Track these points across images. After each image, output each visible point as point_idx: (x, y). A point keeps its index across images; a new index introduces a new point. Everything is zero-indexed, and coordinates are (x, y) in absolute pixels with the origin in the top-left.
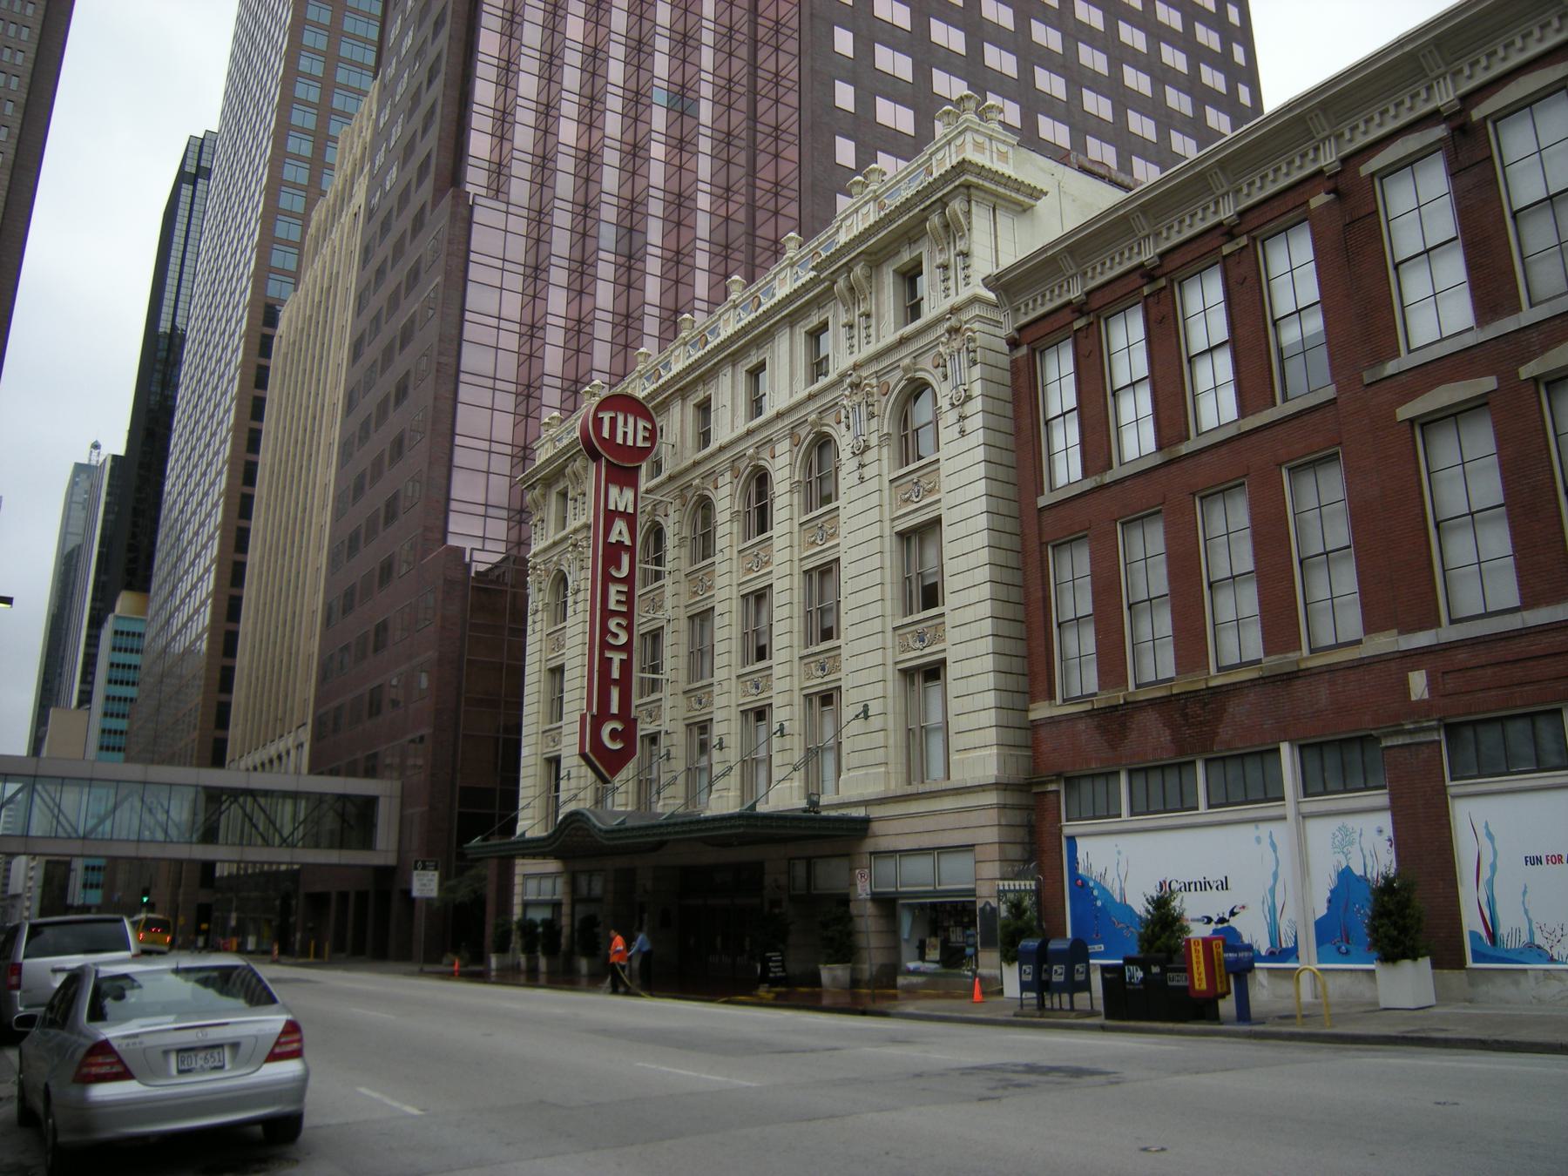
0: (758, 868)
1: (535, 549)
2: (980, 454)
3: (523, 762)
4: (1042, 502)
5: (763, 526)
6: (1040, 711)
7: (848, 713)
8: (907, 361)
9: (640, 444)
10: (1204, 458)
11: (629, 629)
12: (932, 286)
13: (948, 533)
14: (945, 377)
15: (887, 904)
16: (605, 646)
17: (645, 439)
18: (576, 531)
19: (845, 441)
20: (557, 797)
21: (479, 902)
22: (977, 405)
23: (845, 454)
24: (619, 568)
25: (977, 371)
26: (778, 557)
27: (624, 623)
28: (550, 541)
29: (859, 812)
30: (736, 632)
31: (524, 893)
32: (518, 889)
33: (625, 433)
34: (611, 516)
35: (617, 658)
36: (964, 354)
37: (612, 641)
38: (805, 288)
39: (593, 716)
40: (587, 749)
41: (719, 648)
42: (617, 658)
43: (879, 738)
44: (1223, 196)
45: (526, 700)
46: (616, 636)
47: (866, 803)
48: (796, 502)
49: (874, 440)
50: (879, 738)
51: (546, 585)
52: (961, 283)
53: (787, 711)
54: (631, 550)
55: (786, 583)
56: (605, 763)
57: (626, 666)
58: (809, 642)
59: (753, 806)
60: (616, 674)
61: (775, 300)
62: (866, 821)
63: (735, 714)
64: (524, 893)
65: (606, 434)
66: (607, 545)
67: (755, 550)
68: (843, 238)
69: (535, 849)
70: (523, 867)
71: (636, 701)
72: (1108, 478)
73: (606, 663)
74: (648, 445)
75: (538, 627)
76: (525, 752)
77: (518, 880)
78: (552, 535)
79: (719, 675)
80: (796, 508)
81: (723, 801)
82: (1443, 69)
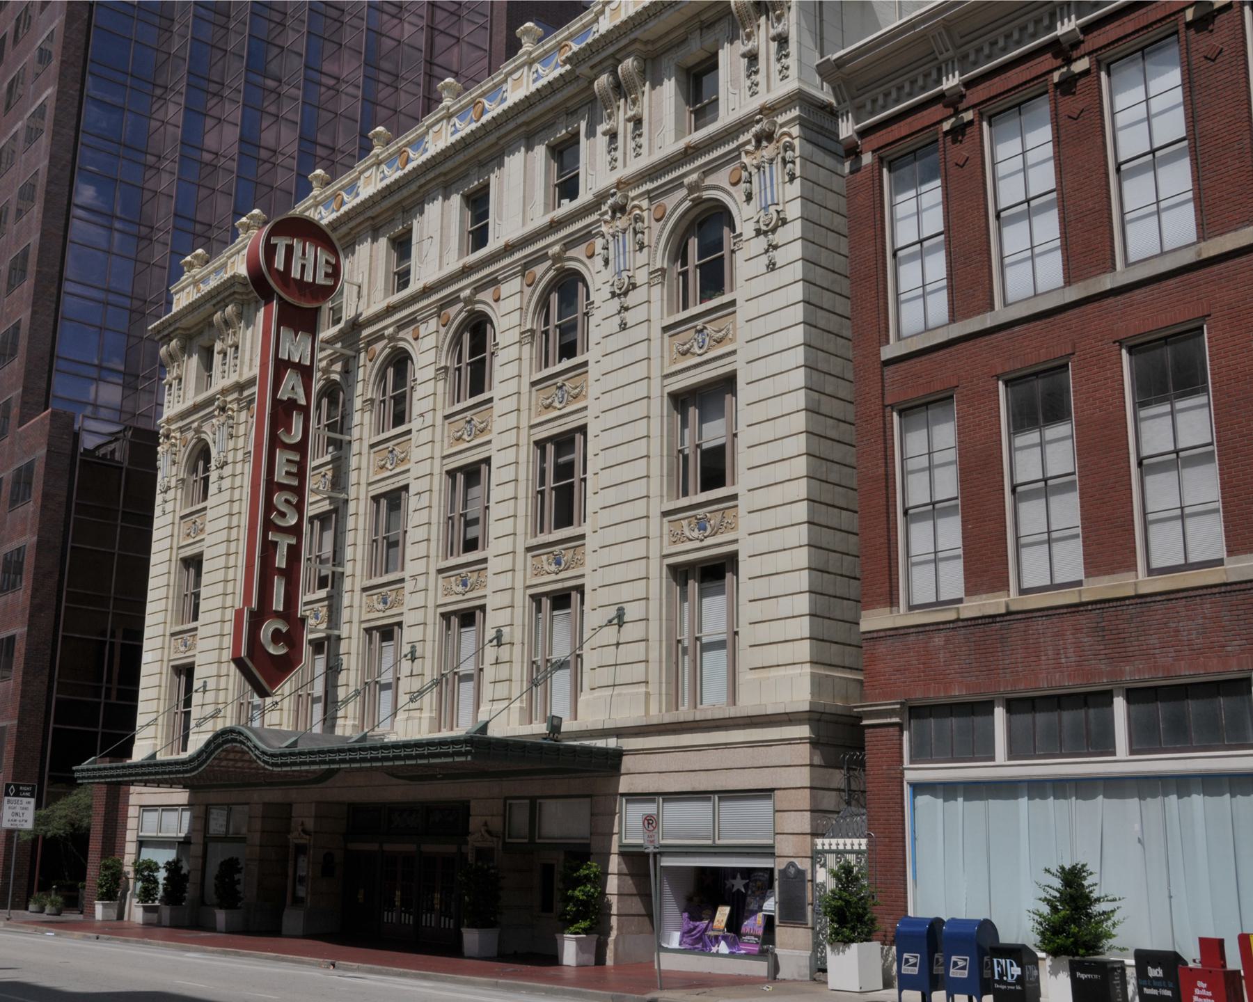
0: (461, 810)
1: (168, 412)
2: (797, 292)
3: (144, 670)
4: (887, 353)
5: (478, 385)
6: (874, 620)
7: (593, 618)
8: (694, 177)
9: (321, 280)
10: (1138, 294)
11: (299, 507)
12: (734, 81)
13: (744, 392)
14: (749, 197)
15: (639, 863)
16: (269, 525)
17: (327, 275)
18: (224, 392)
19: (599, 279)
20: (188, 714)
21: (78, 839)
22: (794, 230)
23: (745, 228)
24: (288, 430)
25: (795, 189)
26: (498, 424)
27: (294, 500)
28: (189, 403)
29: (612, 743)
30: (437, 515)
31: (140, 828)
32: (132, 823)
33: (303, 266)
34: (282, 366)
35: (284, 542)
36: (629, 235)
37: (281, 523)
38: (552, 88)
39: (252, 613)
40: (243, 653)
41: (413, 535)
42: (284, 542)
43: (638, 651)
44: (946, 61)
45: (151, 596)
46: (283, 515)
47: (619, 733)
48: (179, 497)
49: (641, 277)
50: (638, 651)
51: (182, 456)
52: (775, 76)
53: (506, 610)
54: (305, 410)
55: (510, 455)
56: (262, 669)
57: (294, 553)
58: (450, 551)
59: (484, 728)
60: (281, 561)
61: (505, 106)
62: (618, 754)
63: (433, 617)
64: (140, 828)
65: (279, 263)
66: (276, 402)
67: (468, 414)
68: (604, 25)
69: (155, 773)
70: (139, 795)
71: (304, 597)
72: (1107, 282)
73: (269, 548)
74: (330, 282)
75: (169, 507)
76: (146, 657)
77: (132, 812)
78: (192, 397)
79: (411, 568)
80: (178, 502)
81: (410, 724)
82: (951, 53)
